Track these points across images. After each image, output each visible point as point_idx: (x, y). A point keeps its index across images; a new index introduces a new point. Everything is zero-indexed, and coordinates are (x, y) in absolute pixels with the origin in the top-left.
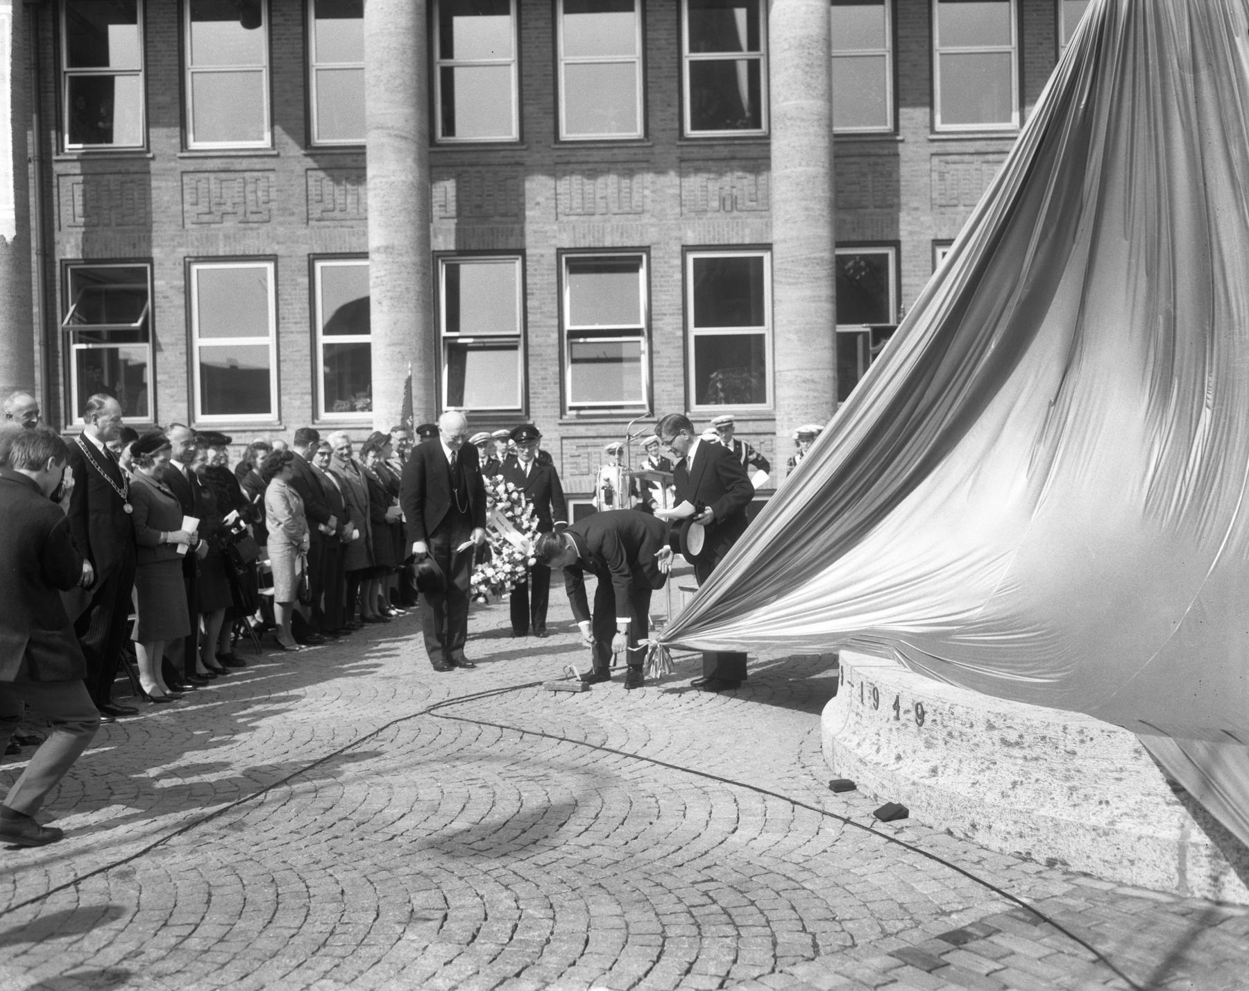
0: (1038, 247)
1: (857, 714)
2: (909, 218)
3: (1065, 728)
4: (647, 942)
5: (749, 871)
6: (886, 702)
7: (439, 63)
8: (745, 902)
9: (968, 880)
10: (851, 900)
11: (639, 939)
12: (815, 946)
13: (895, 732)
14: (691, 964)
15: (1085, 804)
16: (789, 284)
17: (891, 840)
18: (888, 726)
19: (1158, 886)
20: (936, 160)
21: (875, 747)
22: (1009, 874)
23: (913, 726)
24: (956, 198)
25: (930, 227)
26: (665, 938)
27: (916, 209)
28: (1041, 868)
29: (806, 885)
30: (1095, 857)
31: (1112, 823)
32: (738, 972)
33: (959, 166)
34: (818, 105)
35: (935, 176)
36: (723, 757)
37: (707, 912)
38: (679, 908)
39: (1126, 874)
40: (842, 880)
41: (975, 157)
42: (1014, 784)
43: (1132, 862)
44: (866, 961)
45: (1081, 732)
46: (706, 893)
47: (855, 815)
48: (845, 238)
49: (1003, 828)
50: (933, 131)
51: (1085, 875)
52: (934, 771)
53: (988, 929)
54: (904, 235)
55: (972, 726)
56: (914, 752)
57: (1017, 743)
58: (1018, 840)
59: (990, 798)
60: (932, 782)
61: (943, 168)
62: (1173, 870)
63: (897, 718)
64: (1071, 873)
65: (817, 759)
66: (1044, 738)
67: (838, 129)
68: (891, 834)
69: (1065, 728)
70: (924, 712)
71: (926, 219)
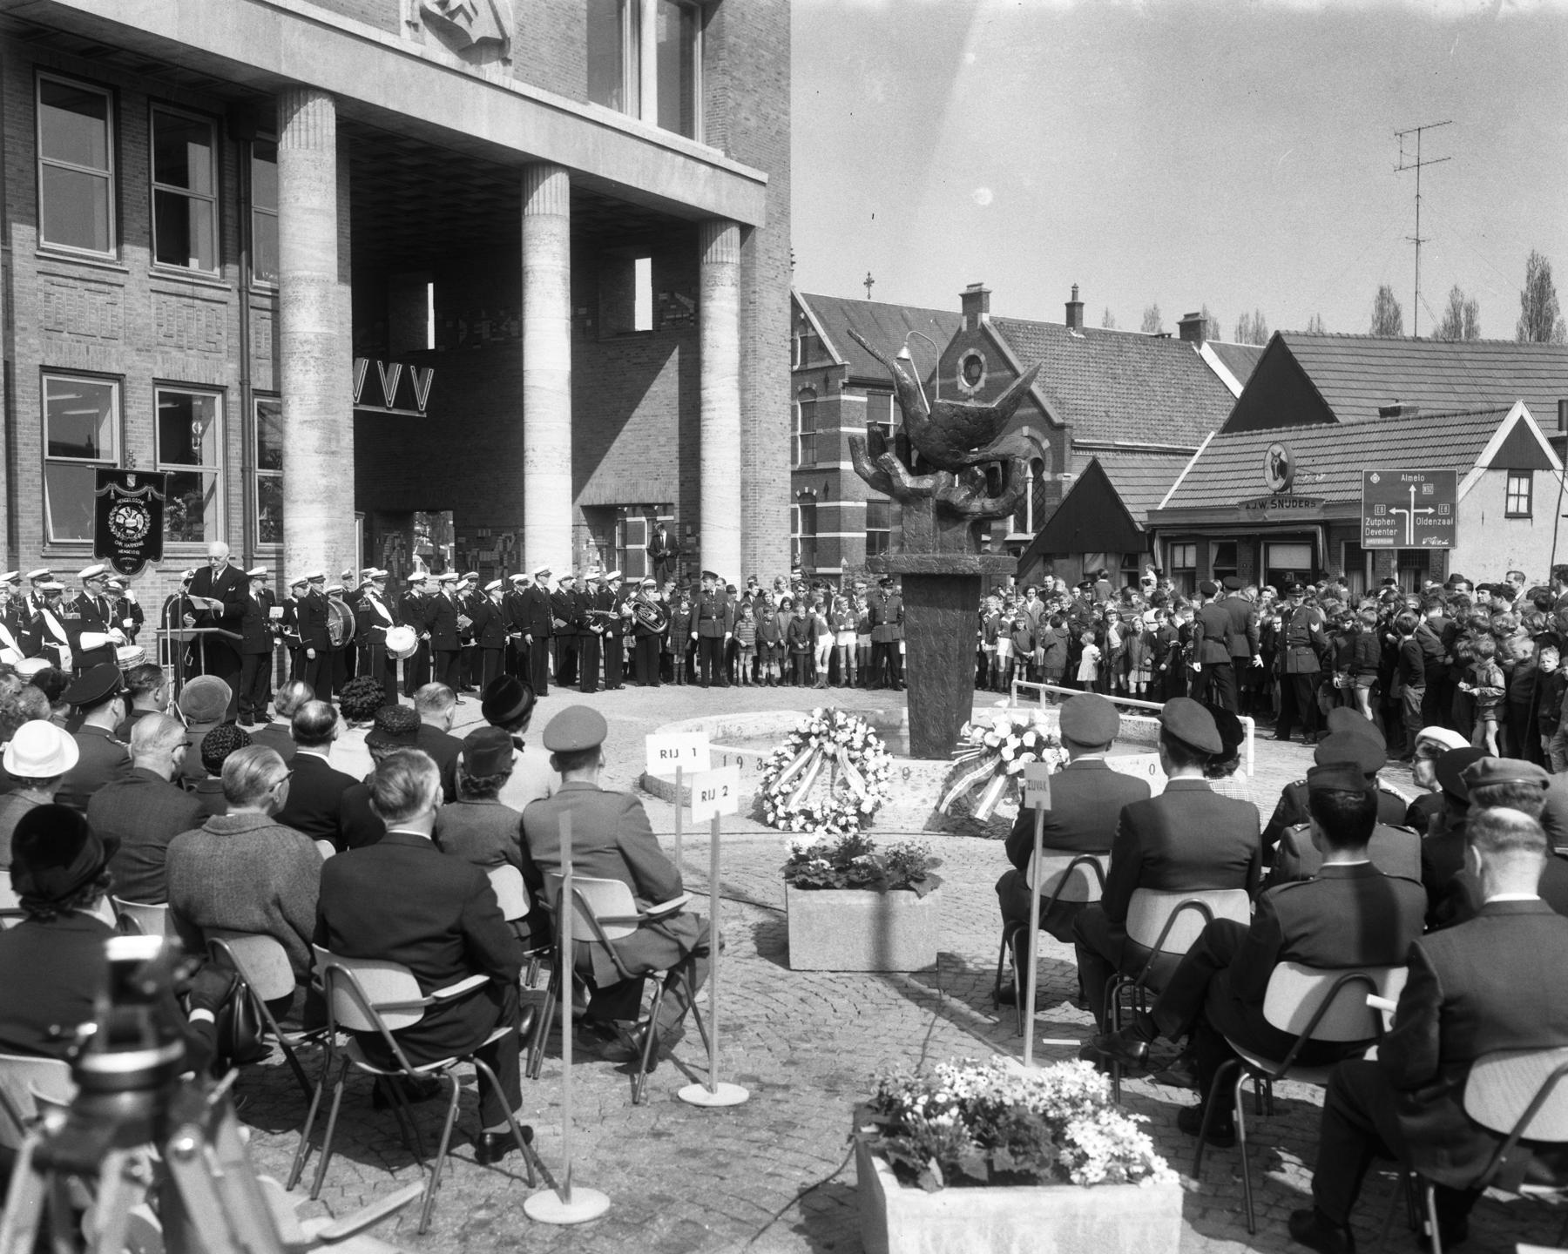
0: (744, 388)
20: (42, 279)
41: (78, 283)
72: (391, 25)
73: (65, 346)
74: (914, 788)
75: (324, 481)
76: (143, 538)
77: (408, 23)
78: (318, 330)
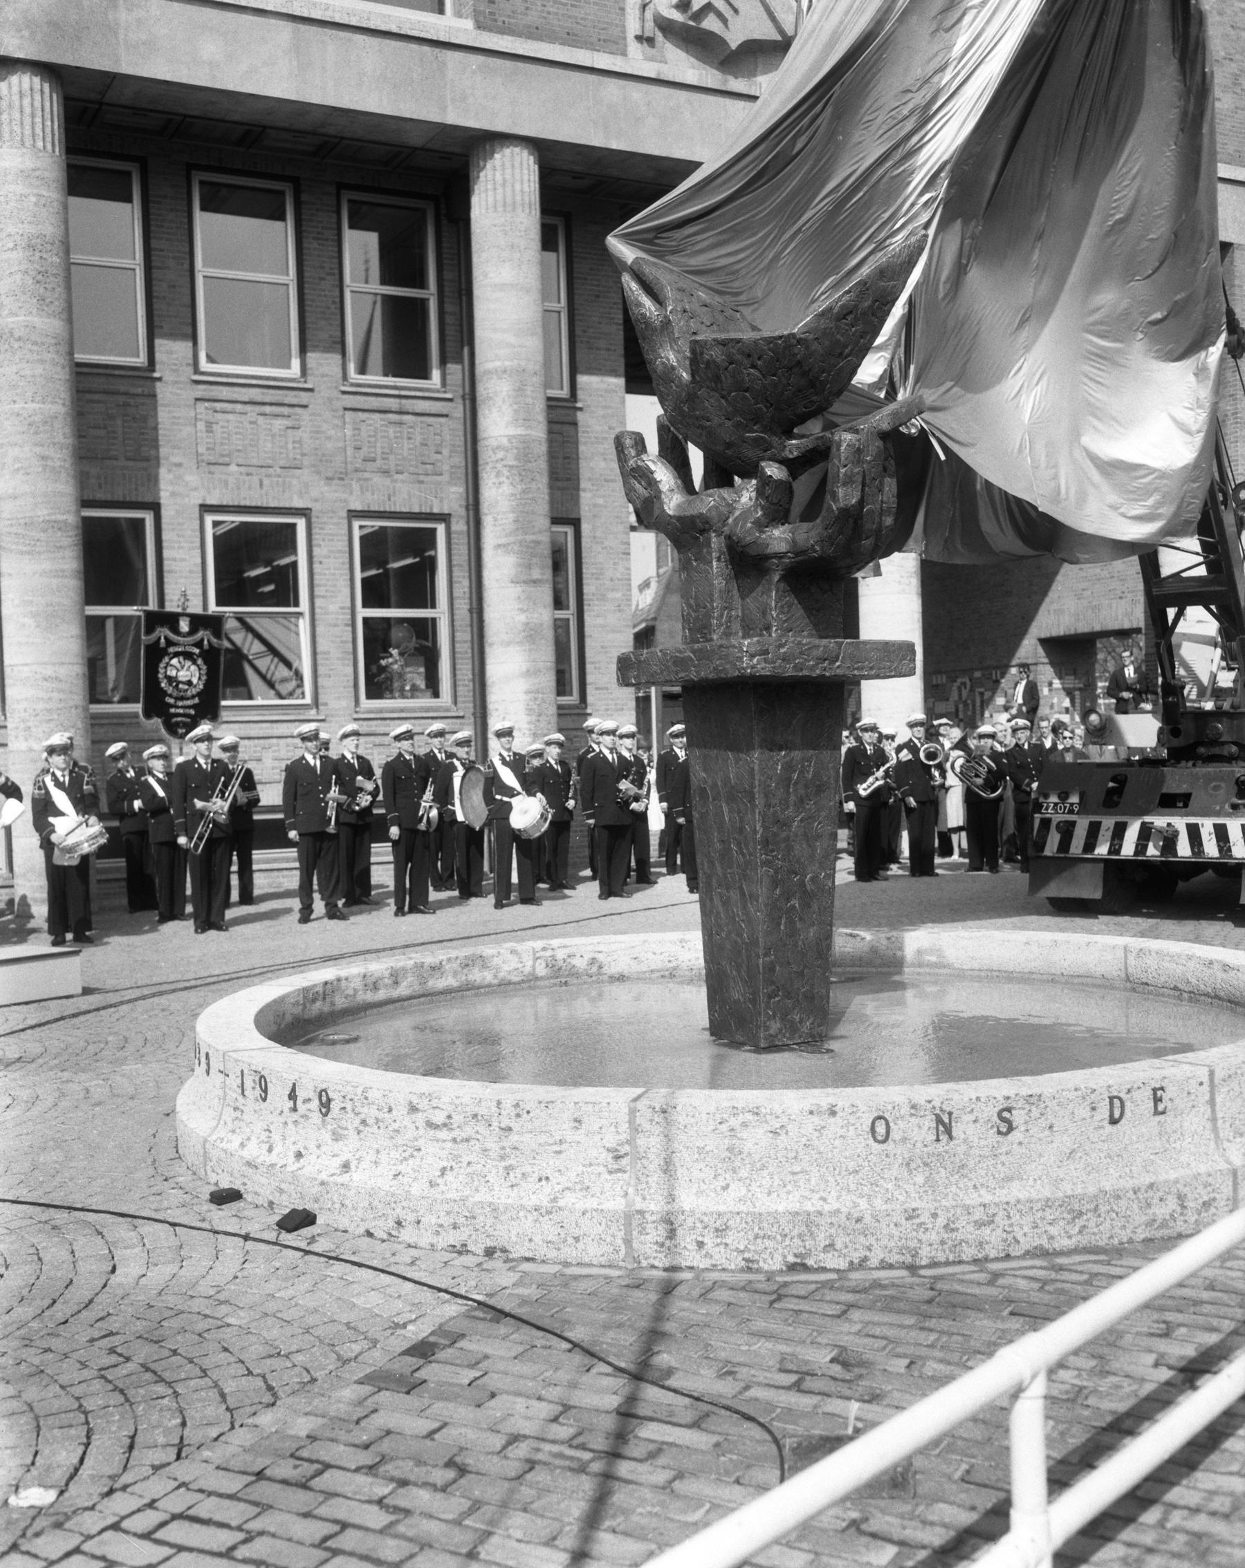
1: (236, 1109)
2: (171, 476)
3: (499, 1103)
4: (66, 1422)
5: (155, 1316)
6: (278, 1093)
7: (569, 614)
8: (166, 1353)
9: (409, 1285)
10: (288, 1331)
11: (51, 1420)
12: (270, 1388)
13: (291, 1126)
14: (133, 1437)
15: (523, 1184)
16: (22, 553)
17: (307, 1252)
18: (282, 1119)
19: (603, 1260)
20: (201, 407)
21: (266, 1147)
22: (450, 1271)
23: (316, 1117)
24: (229, 455)
25: (196, 489)
26: (86, 1413)
27: (180, 465)
28: (481, 1259)
29: (230, 1320)
30: (537, 1239)
31: (555, 1200)
32: (192, 1435)
33: (230, 417)
34: (55, 326)
35: (201, 426)
36: (58, 1179)
37: (125, 1372)
38: (86, 1374)
39: (570, 1253)
40: (271, 1307)
41: (248, 408)
42: (443, 1171)
43: (577, 1239)
44: (335, 1395)
45: (517, 1105)
46: (112, 1351)
47: (253, 1228)
48: (89, 495)
49: (434, 1221)
50: (197, 370)
51: (528, 1259)
52: (346, 1166)
53: (451, 1336)
54: (165, 498)
55: (390, 1110)
56: (319, 1147)
57: (445, 1125)
58: (452, 1232)
59: (416, 1190)
60: (345, 1178)
61: (210, 416)
62: (619, 1242)
63: (295, 1109)
64: (513, 1260)
65: (179, 1168)
66: (475, 1116)
67: (80, 357)
68: (303, 1245)
69: (499, 1103)
70: (329, 1100)
71: (192, 478)
72: (616, 46)
73: (231, 480)
74: (337, 1137)
75: (522, 618)
76: (199, 694)
77: (639, 38)
78: (512, 431)
